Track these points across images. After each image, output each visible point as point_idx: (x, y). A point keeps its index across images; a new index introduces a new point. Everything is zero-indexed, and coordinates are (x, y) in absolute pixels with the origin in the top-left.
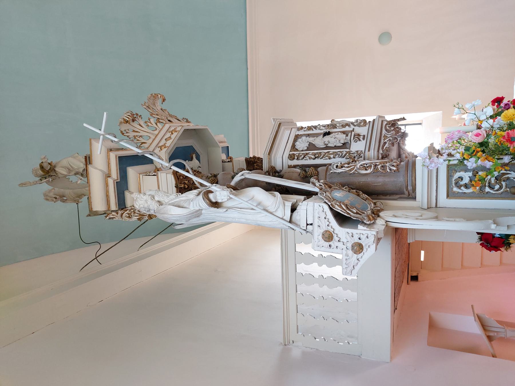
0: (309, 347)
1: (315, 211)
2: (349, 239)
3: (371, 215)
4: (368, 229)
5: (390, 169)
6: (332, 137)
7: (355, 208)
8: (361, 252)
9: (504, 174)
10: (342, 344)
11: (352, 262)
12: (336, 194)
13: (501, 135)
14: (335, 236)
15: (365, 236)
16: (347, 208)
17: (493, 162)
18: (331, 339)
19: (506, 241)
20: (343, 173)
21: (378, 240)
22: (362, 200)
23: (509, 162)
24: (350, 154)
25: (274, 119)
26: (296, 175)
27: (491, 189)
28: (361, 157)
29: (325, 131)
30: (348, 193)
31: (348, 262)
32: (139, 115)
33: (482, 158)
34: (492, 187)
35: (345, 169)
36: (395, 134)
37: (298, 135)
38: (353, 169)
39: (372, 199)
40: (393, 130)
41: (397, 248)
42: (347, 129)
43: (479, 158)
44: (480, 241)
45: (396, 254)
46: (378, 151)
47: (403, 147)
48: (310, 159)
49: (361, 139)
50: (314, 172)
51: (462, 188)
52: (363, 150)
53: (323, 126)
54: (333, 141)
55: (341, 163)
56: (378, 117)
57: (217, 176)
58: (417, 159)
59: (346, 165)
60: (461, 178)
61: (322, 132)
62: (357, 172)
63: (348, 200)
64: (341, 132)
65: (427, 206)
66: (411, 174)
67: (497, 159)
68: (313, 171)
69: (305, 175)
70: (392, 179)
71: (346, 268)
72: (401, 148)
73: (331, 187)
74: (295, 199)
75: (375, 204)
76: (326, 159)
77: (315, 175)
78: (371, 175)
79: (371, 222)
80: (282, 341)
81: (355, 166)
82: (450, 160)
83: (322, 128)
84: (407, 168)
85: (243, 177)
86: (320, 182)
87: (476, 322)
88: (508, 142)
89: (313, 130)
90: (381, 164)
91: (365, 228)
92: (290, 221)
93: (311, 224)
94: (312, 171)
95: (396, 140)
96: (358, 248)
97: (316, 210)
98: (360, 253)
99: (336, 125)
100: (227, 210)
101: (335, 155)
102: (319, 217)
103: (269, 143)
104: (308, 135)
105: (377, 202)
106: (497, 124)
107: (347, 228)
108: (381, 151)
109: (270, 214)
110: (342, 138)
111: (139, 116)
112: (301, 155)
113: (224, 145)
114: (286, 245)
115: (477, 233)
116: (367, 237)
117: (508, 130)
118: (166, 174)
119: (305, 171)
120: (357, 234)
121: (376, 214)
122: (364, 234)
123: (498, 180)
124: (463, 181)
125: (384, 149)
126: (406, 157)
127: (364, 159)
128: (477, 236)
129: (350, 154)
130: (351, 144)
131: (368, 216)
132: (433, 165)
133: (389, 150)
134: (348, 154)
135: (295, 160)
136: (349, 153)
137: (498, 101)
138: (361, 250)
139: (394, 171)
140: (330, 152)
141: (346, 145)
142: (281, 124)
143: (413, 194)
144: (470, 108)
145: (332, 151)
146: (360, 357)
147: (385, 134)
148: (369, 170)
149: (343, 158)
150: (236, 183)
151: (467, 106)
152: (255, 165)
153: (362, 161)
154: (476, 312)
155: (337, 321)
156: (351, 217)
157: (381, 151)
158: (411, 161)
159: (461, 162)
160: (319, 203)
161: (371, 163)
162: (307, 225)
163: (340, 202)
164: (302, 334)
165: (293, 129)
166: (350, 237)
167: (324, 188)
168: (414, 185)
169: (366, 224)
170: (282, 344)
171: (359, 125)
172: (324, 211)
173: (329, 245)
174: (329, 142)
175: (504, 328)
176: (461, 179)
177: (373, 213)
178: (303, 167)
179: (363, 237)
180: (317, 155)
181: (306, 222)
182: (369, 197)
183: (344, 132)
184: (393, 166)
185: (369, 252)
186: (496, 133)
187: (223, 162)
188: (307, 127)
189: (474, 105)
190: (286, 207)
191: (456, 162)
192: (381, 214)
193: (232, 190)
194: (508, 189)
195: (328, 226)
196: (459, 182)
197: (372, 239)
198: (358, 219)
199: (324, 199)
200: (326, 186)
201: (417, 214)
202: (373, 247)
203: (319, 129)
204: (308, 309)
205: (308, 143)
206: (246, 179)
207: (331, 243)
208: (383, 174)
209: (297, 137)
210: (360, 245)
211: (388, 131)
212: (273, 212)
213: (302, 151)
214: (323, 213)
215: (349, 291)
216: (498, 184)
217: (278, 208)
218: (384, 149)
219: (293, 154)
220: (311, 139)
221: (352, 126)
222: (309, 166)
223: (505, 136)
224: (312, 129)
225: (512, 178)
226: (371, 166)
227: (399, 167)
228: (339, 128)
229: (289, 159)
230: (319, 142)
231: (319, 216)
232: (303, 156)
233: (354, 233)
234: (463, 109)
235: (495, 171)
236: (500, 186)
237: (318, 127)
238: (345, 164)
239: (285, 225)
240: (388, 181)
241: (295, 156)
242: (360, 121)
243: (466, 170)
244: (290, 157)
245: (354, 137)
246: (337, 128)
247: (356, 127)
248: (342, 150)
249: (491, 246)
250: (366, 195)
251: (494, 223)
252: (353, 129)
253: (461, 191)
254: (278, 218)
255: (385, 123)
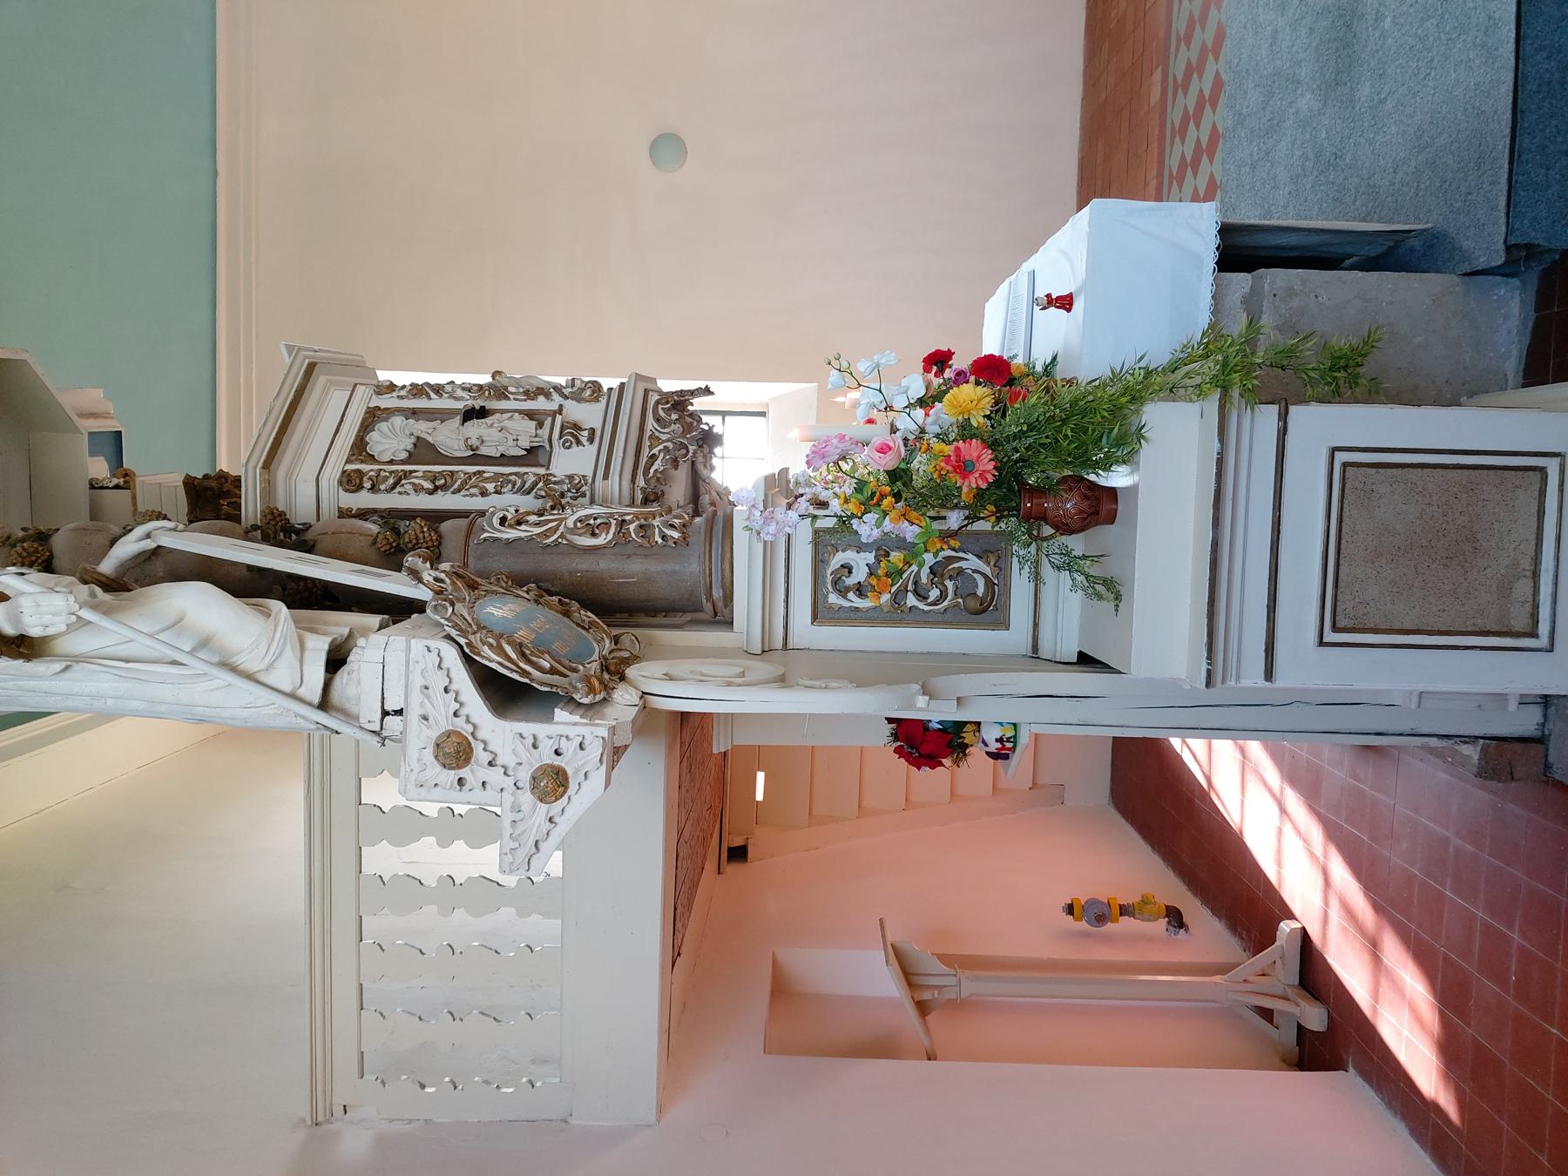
0: (398, 1120)
1: (411, 668)
2: (524, 755)
3: (596, 677)
4: (585, 721)
5: (664, 537)
6: (492, 425)
7: (546, 656)
8: (562, 796)
9: (950, 560)
10: (511, 1090)
11: (532, 829)
12: (490, 609)
13: (940, 452)
14: (478, 748)
15: (574, 743)
16: (523, 655)
17: (921, 527)
18: (477, 1079)
19: (955, 739)
20: (520, 542)
21: (616, 753)
22: (579, 629)
23: (960, 529)
24: (547, 482)
25: (290, 348)
26: (364, 542)
27: (921, 599)
28: (584, 495)
29: (470, 403)
30: (532, 605)
31: (517, 833)
33: (893, 514)
34: (922, 593)
35: (528, 529)
36: (683, 432)
37: (378, 408)
38: (556, 529)
39: (608, 625)
40: (676, 420)
41: (685, 771)
42: (541, 404)
43: (885, 514)
44: (894, 741)
45: (684, 789)
46: (632, 481)
47: (704, 472)
48: (416, 491)
49: (584, 440)
50: (427, 535)
51: (851, 595)
52: (590, 474)
53: (464, 389)
54: (496, 439)
55: (517, 511)
56: (633, 377)
57: (50, 535)
58: (736, 508)
59: (533, 518)
60: (848, 569)
61: (460, 405)
62: (565, 542)
63: (528, 627)
64: (520, 412)
65: (760, 646)
66: (720, 552)
67: (930, 518)
68: (423, 532)
69: (394, 544)
70: (669, 567)
71: (513, 851)
72: (700, 477)
73: (476, 585)
74: (346, 626)
75: (616, 640)
76: (473, 495)
77: (430, 544)
78: (607, 551)
79: (594, 699)
80: (305, 1112)
81: (561, 520)
82: (815, 517)
83: (459, 393)
84: (708, 535)
85: (149, 545)
86: (437, 569)
87: (890, 968)
88: (957, 473)
89: (429, 398)
90: (638, 519)
91: (577, 718)
92: (324, 704)
93: (399, 712)
94: (418, 531)
95: (684, 451)
96: (552, 783)
97: (417, 662)
98: (557, 799)
99: (506, 388)
100: (67, 668)
101: (502, 483)
102: (427, 688)
103: (269, 425)
104: (414, 413)
105: (623, 634)
106: (934, 423)
107: (519, 720)
108: (641, 482)
109: (245, 680)
110: (524, 433)
112: (386, 478)
113: (100, 427)
114: (327, 782)
115: (886, 719)
116: (581, 746)
117: (958, 441)
119: (396, 531)
120: (552, 738)
121: (614, 671)
122: (571, 736)
123: (935, 577)
124: (853, 575)
125: (651, 475)
126: (713, 504)
127: (592, 502)
128: (888, 729)
129: (547, 482)
130: (551, 452)
131: (587, 679)
132: (772, 528)
133: (665, 479)
134: (541, 484)
135: (364, 493)
136: (546, 479)
137: (938, 360)
138: (561, 789)
139: (675, 543)
140: (484, 472)
141: (537, 456)
142: (316, 367)
143: (726, 612)
144: (866, 374)
145: (490, 470)
146: (566, 1122)
147: (654, 430)
148: (603, 536)
149: (529, 493)
150: (121, 565)
151: (862, 367)
152: (222, 502)
153: (582, 506)
154: (890, 939)
155: (495, 1018)
156: (534, 685)
157: (641, 482)
158: (722, 514)
159: (844, 522)
160: (427, 638)
161: (608, 515)
162: (385, 713)
163: (499, 637)
164: (376, 1080)
165: (360, 390)
166: (528, 750)
167: (450, 588)
168: (728, 585)
169: (580, 704)
170: (304, 1121)
171: (577, 397)
172: (444, 666)
173: (457, 778)
174: (483, 442)
175: (956, 975)
176: (847, 570)
177: (605, 667)
178: (390, 518)
179: (569, 748)
180: (443, 481)
181: (380, 704)
182: (599, 618)
183: (530, 415)
184: (672, 526)
185: (586, 794)
186: (929, 448)
187: (92, 487)
188: (411, 385)
189: (878, 366)
190: (307, 655)
191: (830, 523)
192: (631, 672)
193: (98, 590)
194: (960, 600)
195: (455, 714)
196: (844, 578)
197: (595, 750)
198: (554, 690)
199: (446, 628)
200: (458, 582)
201: (729, 669)
202: (599, 776)
203: (452, 397)
204: (408, 988)
205: (413, 439)
206: (171, 552)
207: (464, 773)
208: (641, 551)
209: (373, 417)
210: (557, 774)
211: (661, 421)
212: (259, 671)
213: (391, 462)
214: (440, 673)
215: (535, 917)
216: (936, 587)
217: (277, 657)
218: (651, 475)
219: (358, 470)
220: (422, 428)
221: (555, 396)
222: (410, 515)
223: (950, 456)
224: (427, 392)
225: (970, 571)
226: (608, 525)
227: (689, 530)
228: (515, 399)
229: (341, 491)
230: (450, 438)
231: (425, 683)
232: (391, 481)
233: (541, 736)
234: (851, 374)
235: (926, 551)
236: (941, 591)
237: (449, 388)
238: (528, 513)
239: (303, 717)
240: (657, 573)
241: (365, 479)
242: (583, 385)
243: (861, 548)
244: (345, 480)
245: (561, 432)
246: (509, 399)
247: (570, 401)
248: (523, 470)
249: (920, 756)
250: (590, 614)
251: (924, 694)
252: (561, 406)
253: (847, 604)
254: (276, 693)
255: (654, 398)
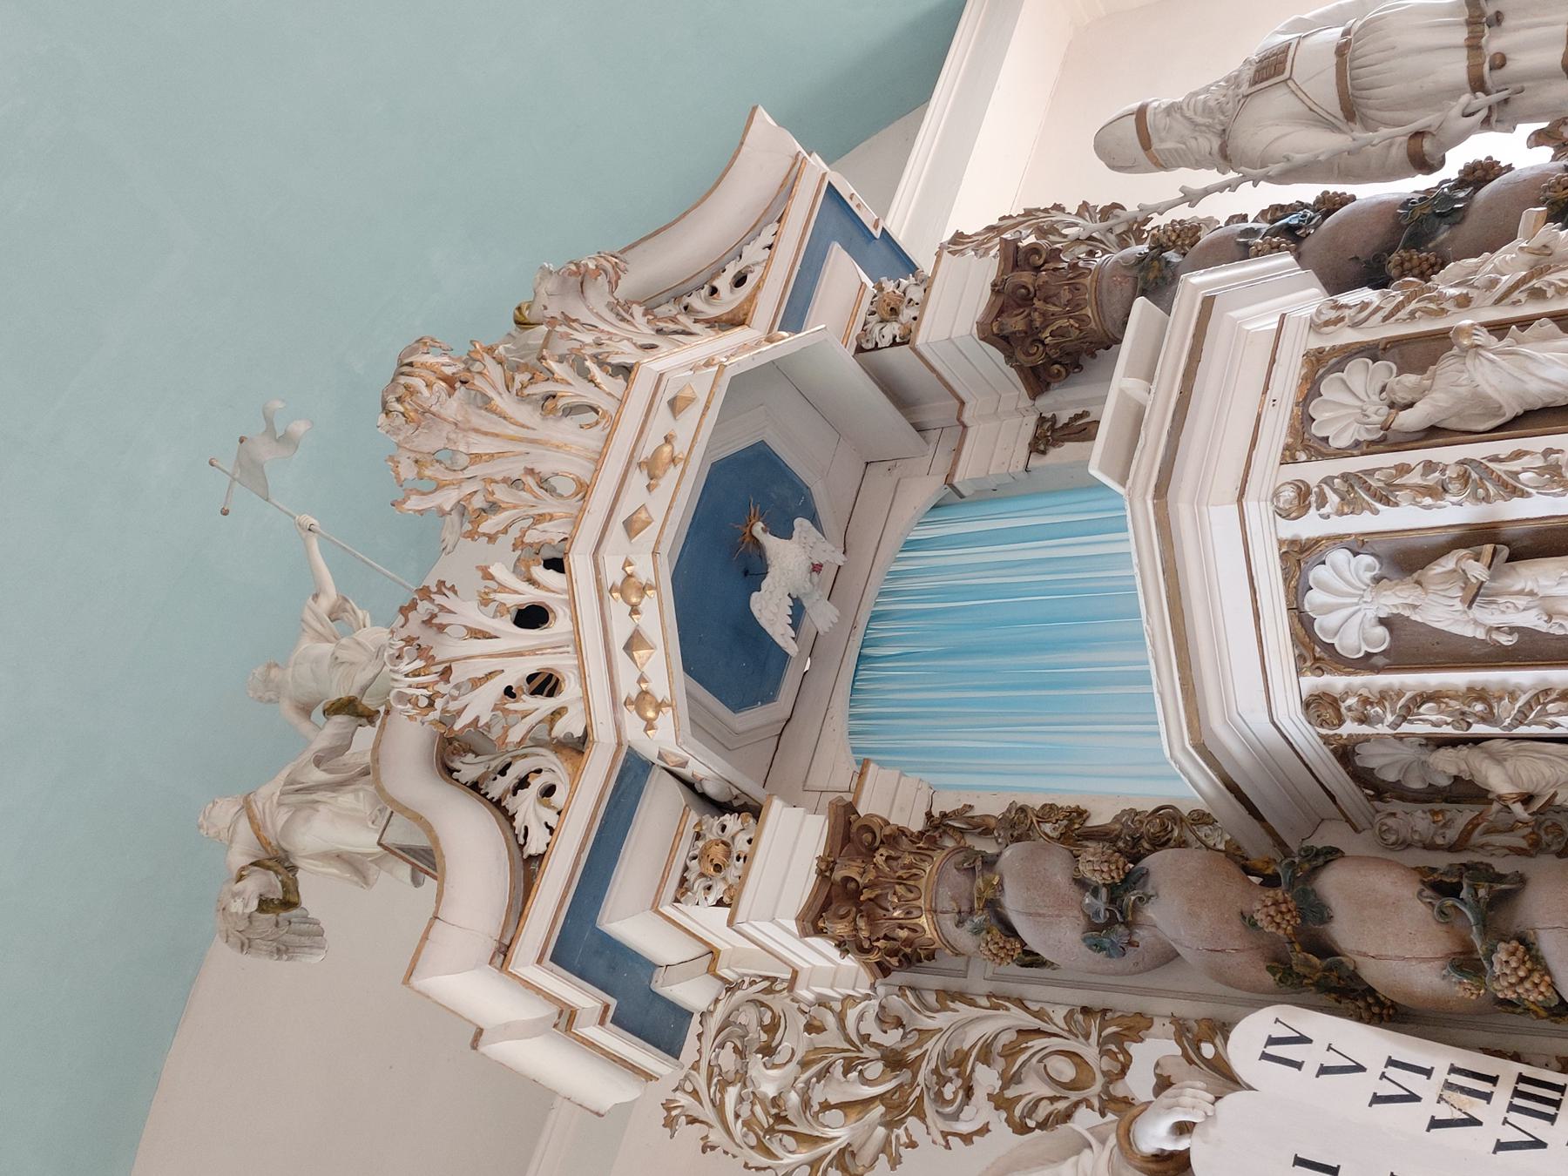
32: (434, 589)
111: (440, 592)
118: (902, 774)
